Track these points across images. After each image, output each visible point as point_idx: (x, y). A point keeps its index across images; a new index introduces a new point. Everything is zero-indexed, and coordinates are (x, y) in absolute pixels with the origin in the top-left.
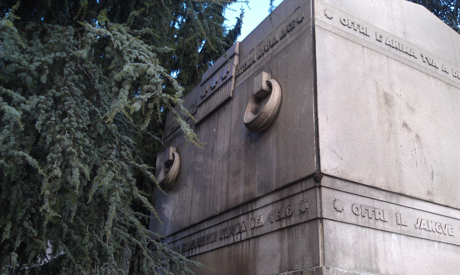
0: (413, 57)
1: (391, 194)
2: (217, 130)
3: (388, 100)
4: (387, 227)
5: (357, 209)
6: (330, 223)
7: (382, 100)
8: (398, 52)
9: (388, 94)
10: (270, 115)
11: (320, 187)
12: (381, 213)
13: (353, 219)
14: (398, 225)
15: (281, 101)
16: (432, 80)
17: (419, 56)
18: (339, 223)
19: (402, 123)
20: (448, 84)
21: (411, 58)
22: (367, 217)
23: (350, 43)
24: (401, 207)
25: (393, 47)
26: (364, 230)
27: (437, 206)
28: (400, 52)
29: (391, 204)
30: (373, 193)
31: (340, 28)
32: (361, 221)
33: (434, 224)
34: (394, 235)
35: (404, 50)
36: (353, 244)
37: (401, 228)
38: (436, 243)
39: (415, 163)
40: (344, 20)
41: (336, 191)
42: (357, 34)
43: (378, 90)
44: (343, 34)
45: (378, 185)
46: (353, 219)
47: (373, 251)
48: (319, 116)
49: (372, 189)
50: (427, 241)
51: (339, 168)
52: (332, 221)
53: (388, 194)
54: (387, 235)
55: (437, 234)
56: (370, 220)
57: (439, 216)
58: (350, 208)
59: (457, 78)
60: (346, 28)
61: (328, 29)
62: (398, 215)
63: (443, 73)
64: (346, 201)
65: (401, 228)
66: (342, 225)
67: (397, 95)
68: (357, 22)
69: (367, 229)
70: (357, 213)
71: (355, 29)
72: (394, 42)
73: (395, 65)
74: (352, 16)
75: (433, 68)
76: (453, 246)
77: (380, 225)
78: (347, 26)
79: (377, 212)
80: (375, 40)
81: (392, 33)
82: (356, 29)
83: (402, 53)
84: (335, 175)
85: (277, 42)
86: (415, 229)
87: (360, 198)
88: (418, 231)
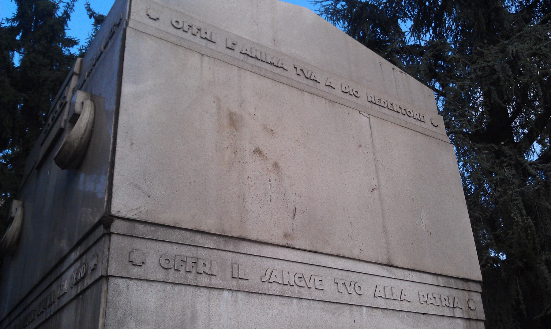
0: (282, 69)
1: (226, 239)
2: (50, 172)
3: (234, 121)
4: (215, 282)
5: (167, 262)
6: (121, 282)
7: (225, 121)
8: (259, 63)
9: (235, 114)
10: (76, 145)
11: (110, 234)
12: (207, 264)
13: (160, 275)
14: (234, 280)
15: (93, 126)
16: (306, 96)
17: (290, 68)
18: (136, 281)
19: (253, 149)
20: (331, 101)
21: (279, 71)
22: (183, 271)
23: (181, 50)
24: (241, 255)
25: (251, 57)
26: (177, 288)
27: (299, 252)
28: (263, 63)
29: (225, 253)
30: (197, 239)
31: (169, 31)
32: (172, 276)
33: (292, 275)
34: (226, 293)
35: (269, 61)
36: (156, 308)
37: (238, 283)
38: (295, 301)
39: (269, 199)
40: (177, 21)
41: (135, 239)
42: (197, 39)
43: (219, 109)
44: (173, 39)
45: (204, 228)
46: (160, 275)
47: (189, 316)
48: (118, 141)
49: (195, 234)
50: (281, 299)
51: (142, 209)
52: (123, 280)
53: (222, 240)
54: (216, 292)
55: (296, 288)
56: (188, 275)
57: (302, 265)
58: (156, 261)
59: (348, 94)
60: (180, 33)
61: (148, 32)
62: (234, 266)
63: (327, 89)
64: (152, 253)
65: (238, 283)
66: (140, 283)
67: (250, 114)
68: (197, 24)
69: (183, 288)
70: (166, 266)
71: (194, 35)
72: (253, 51)
73: (250, 79)
74: (192, 18)
75: (312, 82)
76: (322, 303)
77: (204, 280)
78: (181, 30)
79: (200, 263)
80: (224, 47)
81: (255, 41)
82: (195, 33)
83: (265, 64)
84: (135, 217)
85: (102, 53)
86: (261, 283)
87: (175, 247)
88: (266, 285)
